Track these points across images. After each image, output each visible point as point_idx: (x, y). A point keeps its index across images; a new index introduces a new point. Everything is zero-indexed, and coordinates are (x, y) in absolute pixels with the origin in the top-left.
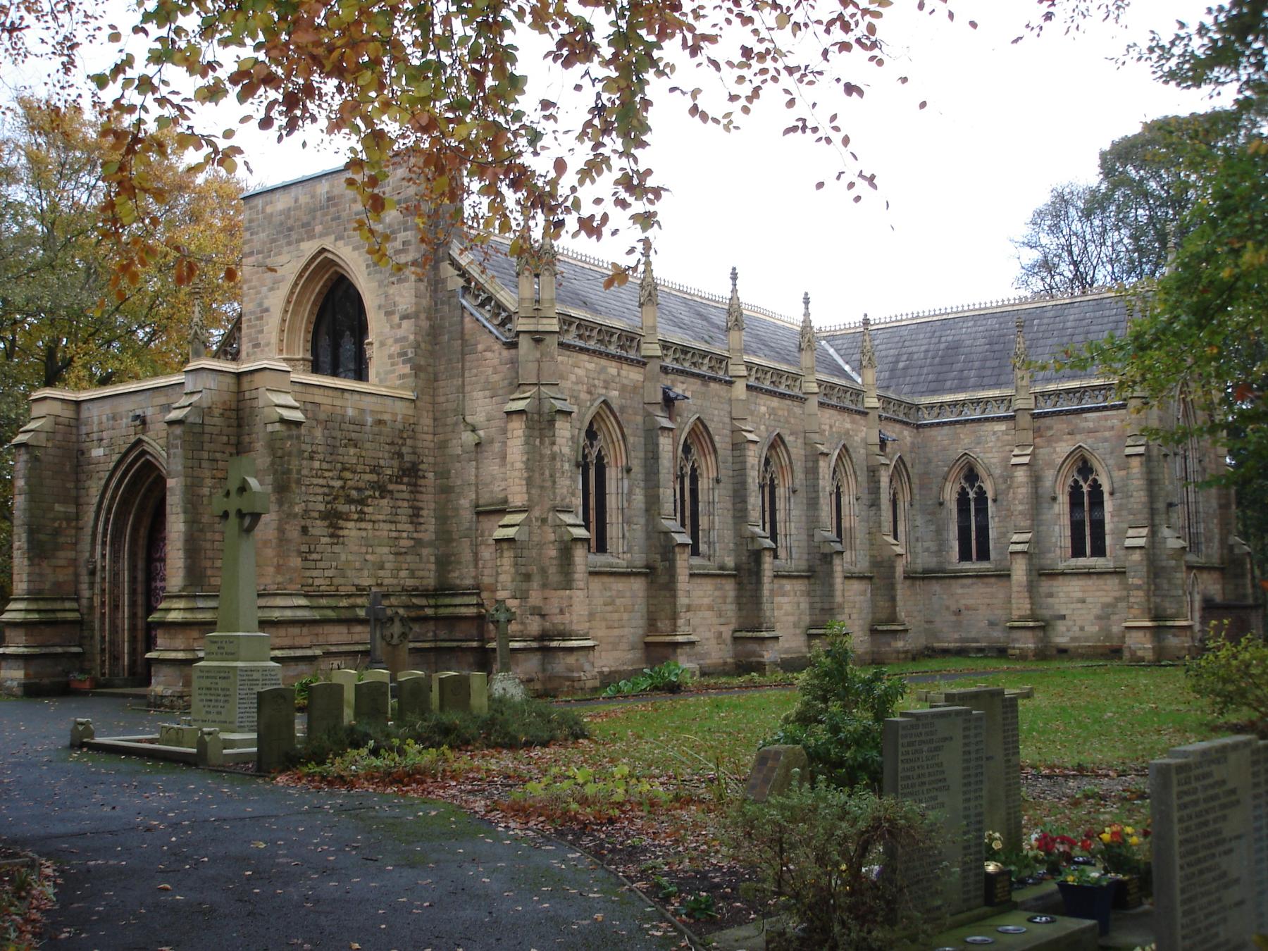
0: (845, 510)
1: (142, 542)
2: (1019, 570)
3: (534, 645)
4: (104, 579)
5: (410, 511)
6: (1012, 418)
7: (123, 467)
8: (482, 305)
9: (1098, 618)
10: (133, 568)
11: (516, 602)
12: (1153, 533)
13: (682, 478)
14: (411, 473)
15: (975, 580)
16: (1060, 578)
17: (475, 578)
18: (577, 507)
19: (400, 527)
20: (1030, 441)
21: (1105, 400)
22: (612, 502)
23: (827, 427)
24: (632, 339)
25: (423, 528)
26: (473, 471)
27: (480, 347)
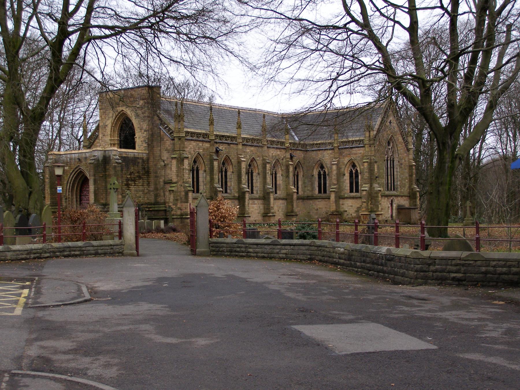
0: (278, 179)
1: (79, 191)
2: (333, 196)
3: (179, 217)
4: (69, 201)
5: (147, 183)
6: (333, 149)
7: (74, 172)
8: (165, 128)
9: (356, 211)
10: (76, 198)
11: (174, 206)
12: (371, 186)
13: (222, 172)
14: (147, 172)
15: (322, 200)
16: (346, 199)
17: (164, 200)
18: (190, 181)
19: (145, 187)
20: (338, 157)
21: (359, 145)
22: (201, 179)
23: (271, 154)
24: (207, 135)
25: (150, 187)
26: (163, 172)
27: (165, 139)
